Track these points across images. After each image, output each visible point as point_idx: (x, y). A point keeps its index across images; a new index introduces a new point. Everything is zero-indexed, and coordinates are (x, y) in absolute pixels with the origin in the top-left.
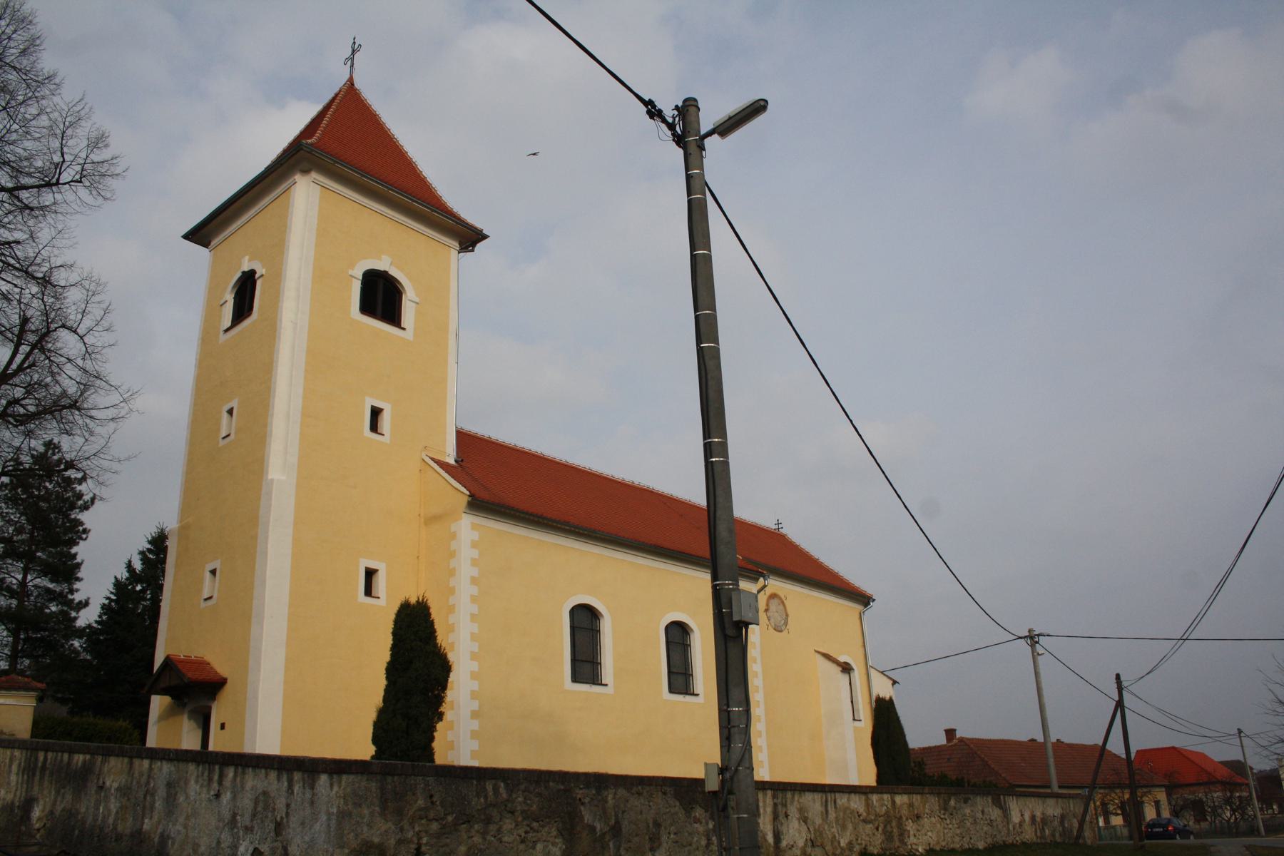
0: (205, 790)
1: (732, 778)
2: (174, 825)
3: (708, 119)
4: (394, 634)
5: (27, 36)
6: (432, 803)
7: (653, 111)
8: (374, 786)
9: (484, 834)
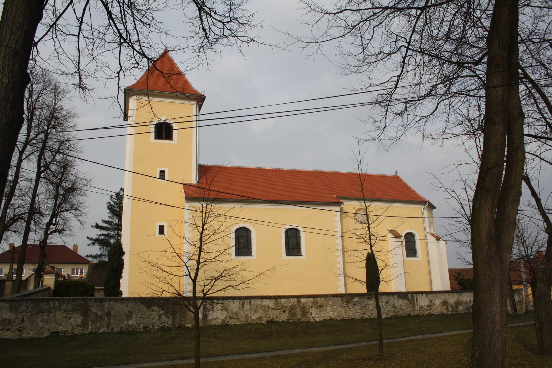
8: (7, 305)
9: (48, 316)
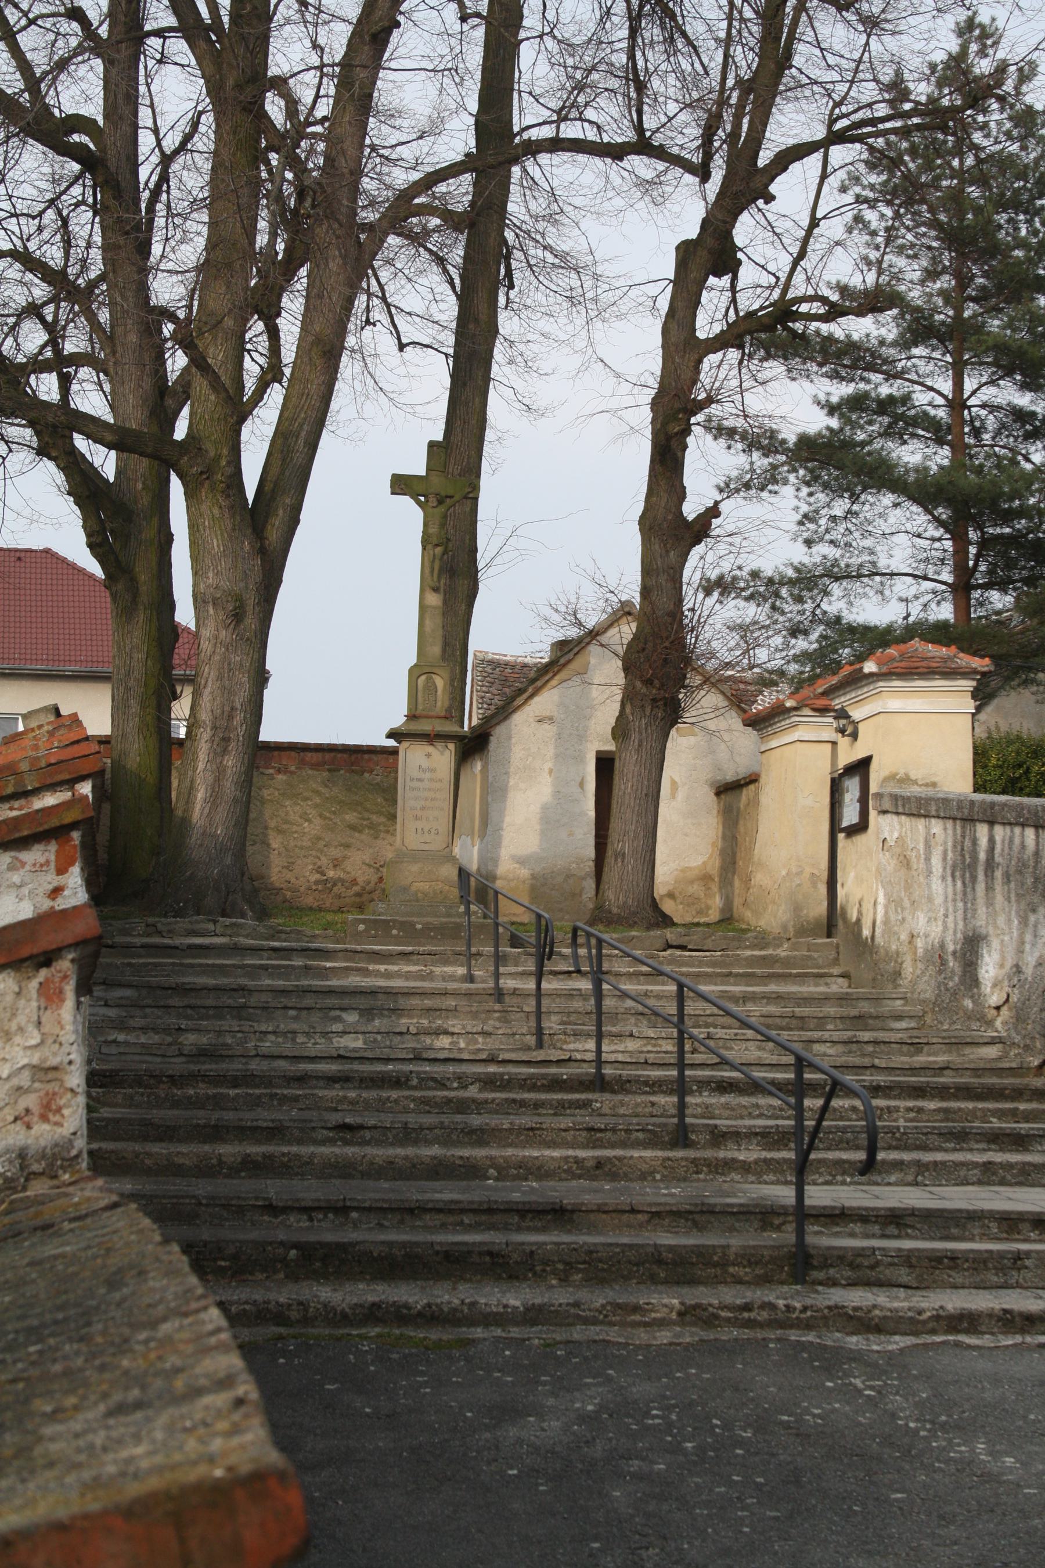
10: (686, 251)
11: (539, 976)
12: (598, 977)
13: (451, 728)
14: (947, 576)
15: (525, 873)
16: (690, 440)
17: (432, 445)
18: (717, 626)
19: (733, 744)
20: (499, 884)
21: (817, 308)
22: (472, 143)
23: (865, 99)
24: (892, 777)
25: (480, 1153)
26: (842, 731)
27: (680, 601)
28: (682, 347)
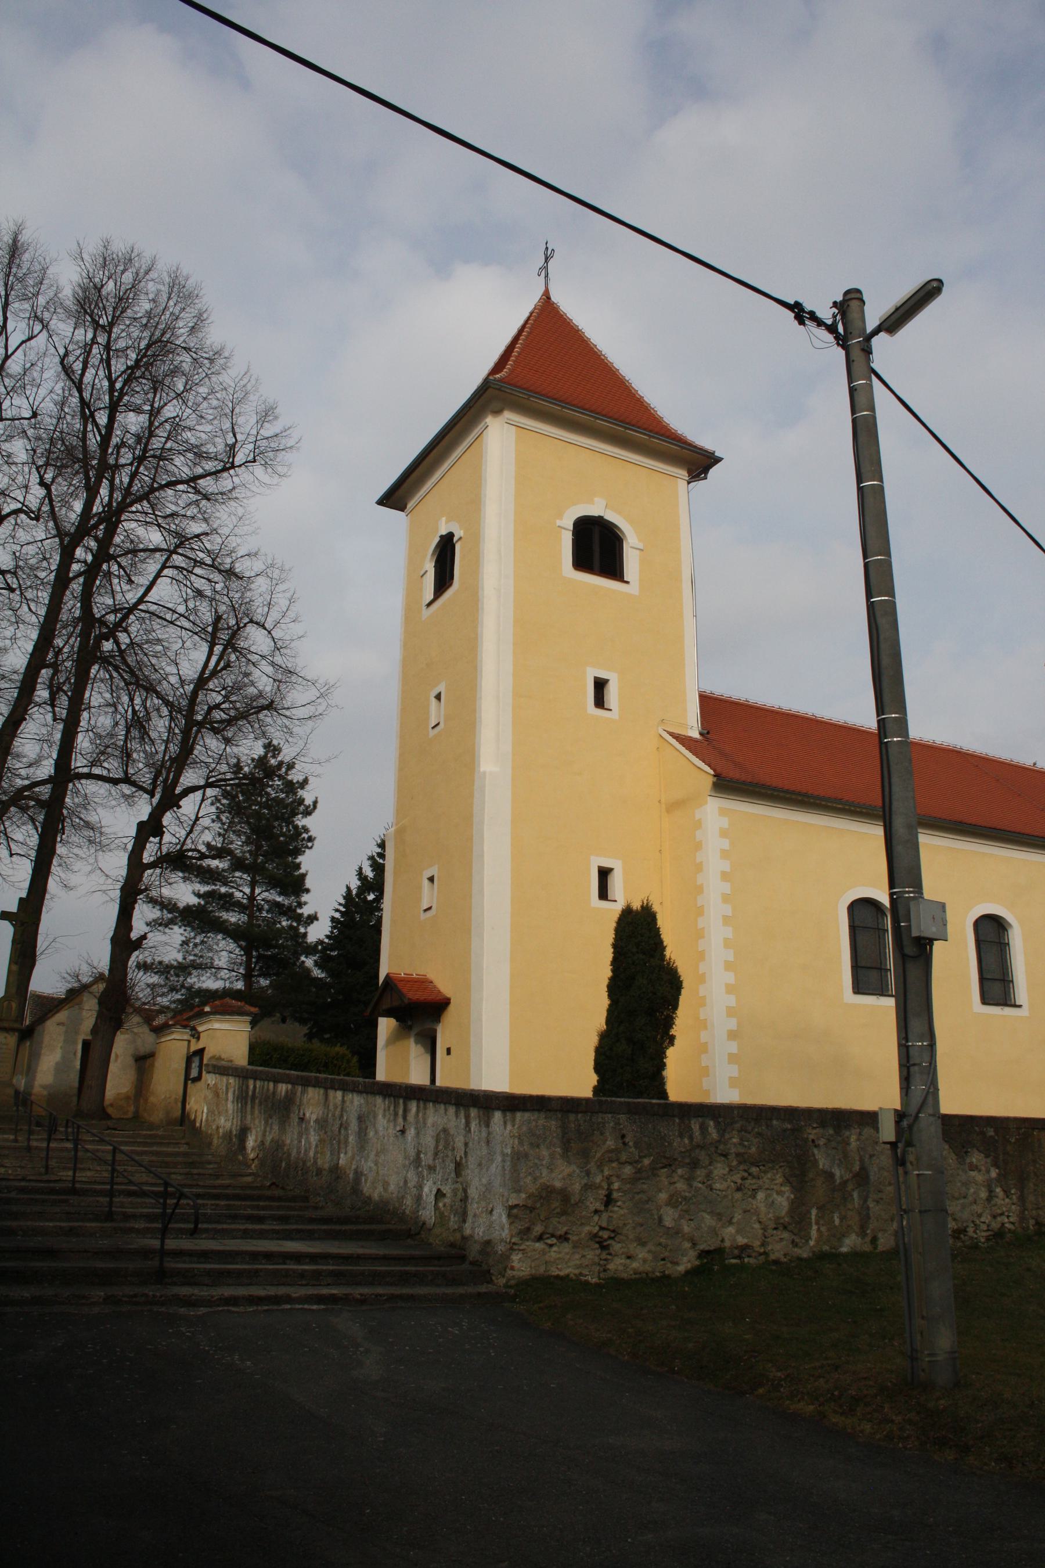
0: (391, 1125)
1: (910, 1127)
2: (366, 1161)
3: (873, 316)
4: (615, 946)
5: (195, 312)
6: (624, 1144)
7: (800, 313)
8: (553, 1124)
9: (689, 1180)
10: (141, 825)
11: (49, 1140)
12: (76, 1142)
13: (16, 1025)
14: (242, 971)
15: (45, 1093)
16: (137, 906)
17: (21, 899)
18: (142, 982)
19: (146, 1038)
20: (33, 1098)
21: (195, 854)
22: (53, 771)
23: (222, 771)
24: (213, 1057)
25: (14, 1224)
26: (193, 1036)
27: (126, 974)
28: (136, 865)
